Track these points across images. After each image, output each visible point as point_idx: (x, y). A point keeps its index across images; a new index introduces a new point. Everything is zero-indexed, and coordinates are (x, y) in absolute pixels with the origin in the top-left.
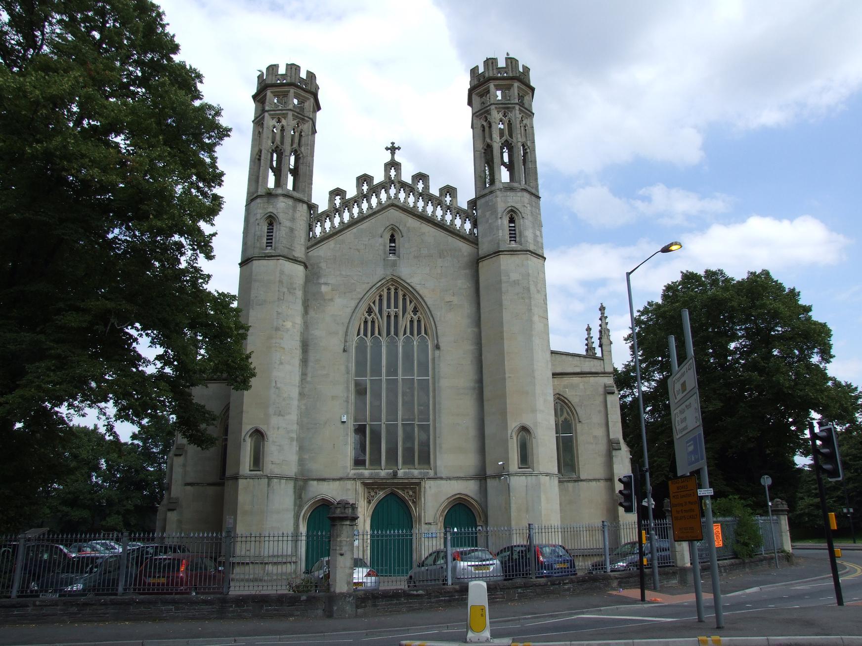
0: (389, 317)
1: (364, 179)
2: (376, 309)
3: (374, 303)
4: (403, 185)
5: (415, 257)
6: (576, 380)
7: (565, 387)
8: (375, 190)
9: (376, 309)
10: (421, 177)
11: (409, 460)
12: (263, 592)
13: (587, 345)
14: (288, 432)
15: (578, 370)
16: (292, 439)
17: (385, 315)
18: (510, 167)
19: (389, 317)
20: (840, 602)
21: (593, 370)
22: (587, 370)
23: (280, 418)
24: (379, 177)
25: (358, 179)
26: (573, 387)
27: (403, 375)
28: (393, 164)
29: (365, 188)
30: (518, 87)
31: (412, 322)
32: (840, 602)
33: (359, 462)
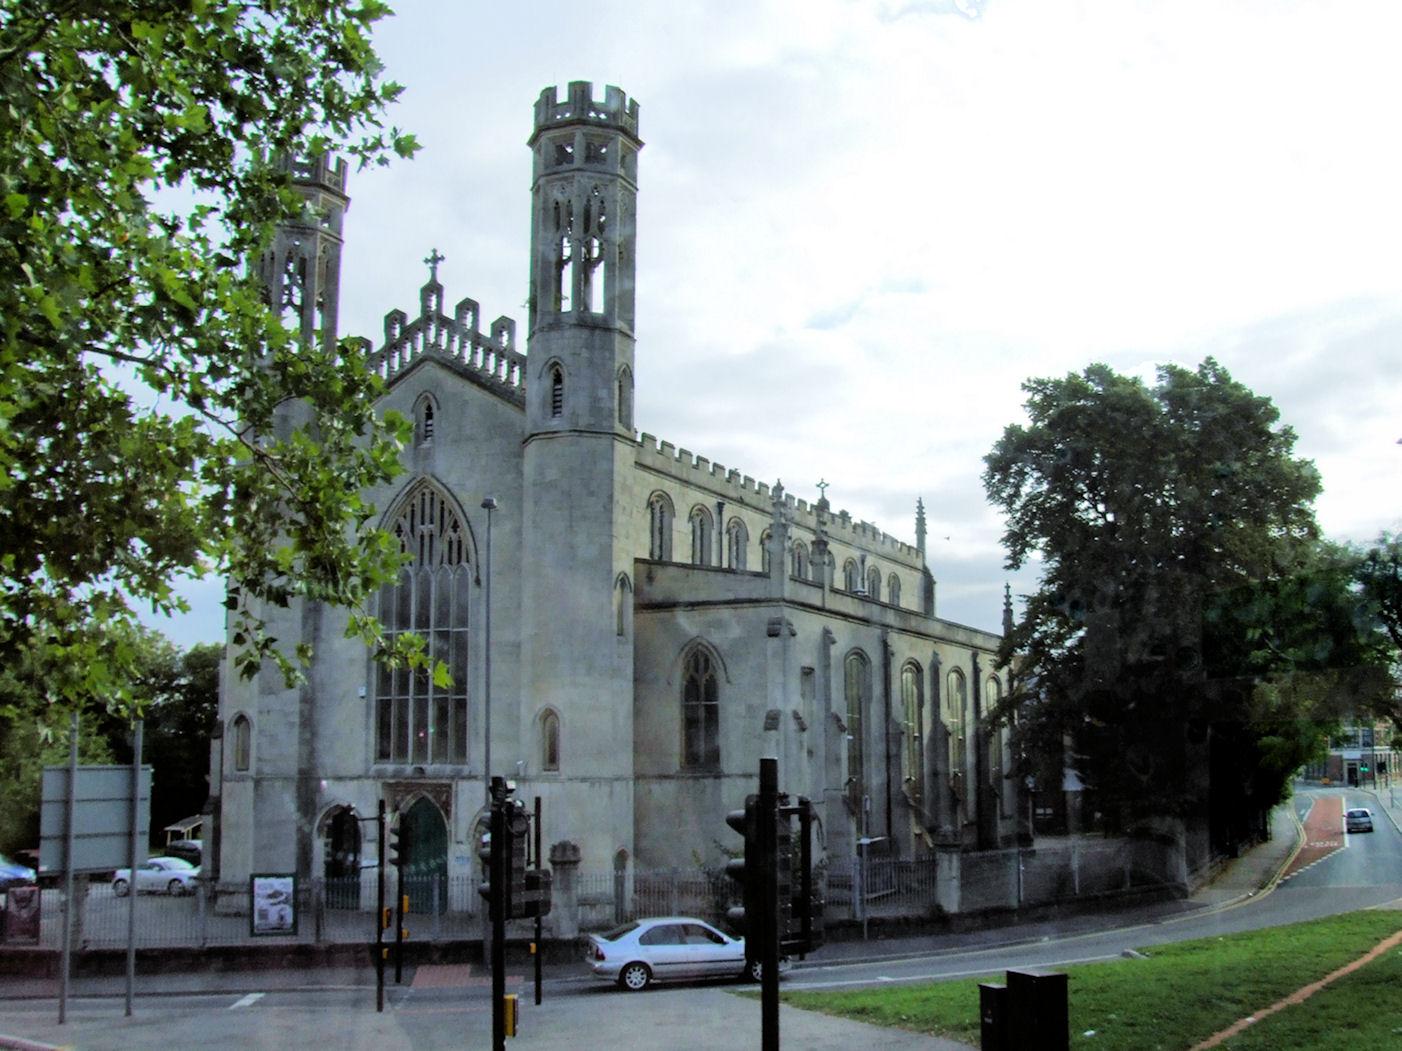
0: (422, 537)
1: (395, 318)
2: (406, 526)
3: (405, 517)
4: (444, 322)
5: (455, 441)
6: (725, 613)
7: (710, 625)
8: (409, 333)
9: (406, 526)
10: (468, 306)
11: (440, 754)
12: (224, 945)
13: (269, 599)
14: (286, 715)
15: (731, 596)
16: (292, 724)
17: (418, 533)
18: (302, 310)
19: (422, 537)
20: (129, 1013)
21: (755, 596)
22: (744, 595)
23: (273, 696)
24: (414, 314)
25: (388, 318)
26: (720, 625)
27: (436, 627)
28: (433, 289)
29: (397, 332)
30: (624, 144)
31: (450, 543)
32: (129, 1013)
33: (383, 755)
